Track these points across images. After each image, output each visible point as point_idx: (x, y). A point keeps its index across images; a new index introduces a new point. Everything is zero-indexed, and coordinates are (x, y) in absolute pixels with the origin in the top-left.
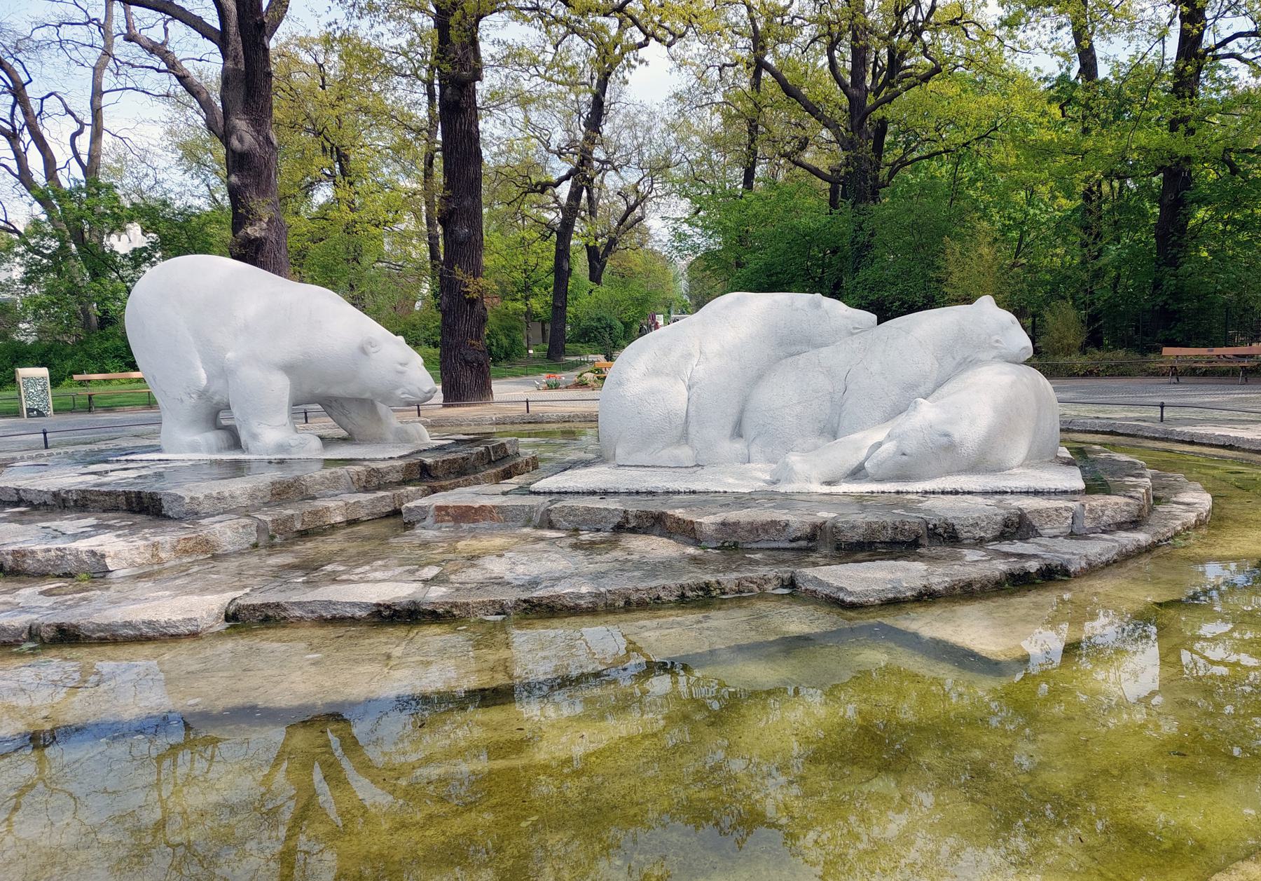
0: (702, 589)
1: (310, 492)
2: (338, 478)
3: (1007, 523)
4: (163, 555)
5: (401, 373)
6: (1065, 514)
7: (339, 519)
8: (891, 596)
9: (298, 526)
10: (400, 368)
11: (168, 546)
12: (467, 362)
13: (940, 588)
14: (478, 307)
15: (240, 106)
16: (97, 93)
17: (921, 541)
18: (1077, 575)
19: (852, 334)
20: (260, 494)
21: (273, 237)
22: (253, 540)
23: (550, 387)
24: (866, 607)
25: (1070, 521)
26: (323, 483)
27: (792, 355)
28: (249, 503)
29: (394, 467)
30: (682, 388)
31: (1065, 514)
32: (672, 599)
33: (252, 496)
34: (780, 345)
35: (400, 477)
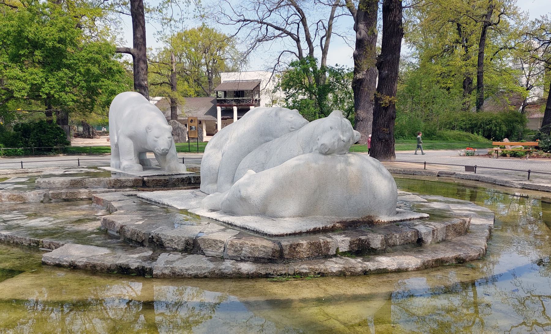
0: (36, 243)
1: (87, 185)
2: (101, 181)
3: (187, 243)
4: (3, 199)
5: (156, 141)
6: (220, 245)
7: (84, 197)
8: (57, 262)
9: (64, 197)
10: (156, 139)
11: (6, 196)
12: (380, 139)
13: (80, 264)
14: (390, 111)
15: (362, 18)
16: (332, 18)
17: (144, 244)
18: (157, 277)
19: (291, 131)
20: (65, 184)
21: (368, 78)
22: (42, 199)
23: (468, 155)
24: (48, 265)
25: (222, 249)
26: (93, 182)
27: (267, 141)
28: (60, 186)
29: (129, 180)
30: (220, 155)
31: (220, 245)
32: (26, 245)
33: (62, 184)
34: (261, 135)
35: (132, 184)
